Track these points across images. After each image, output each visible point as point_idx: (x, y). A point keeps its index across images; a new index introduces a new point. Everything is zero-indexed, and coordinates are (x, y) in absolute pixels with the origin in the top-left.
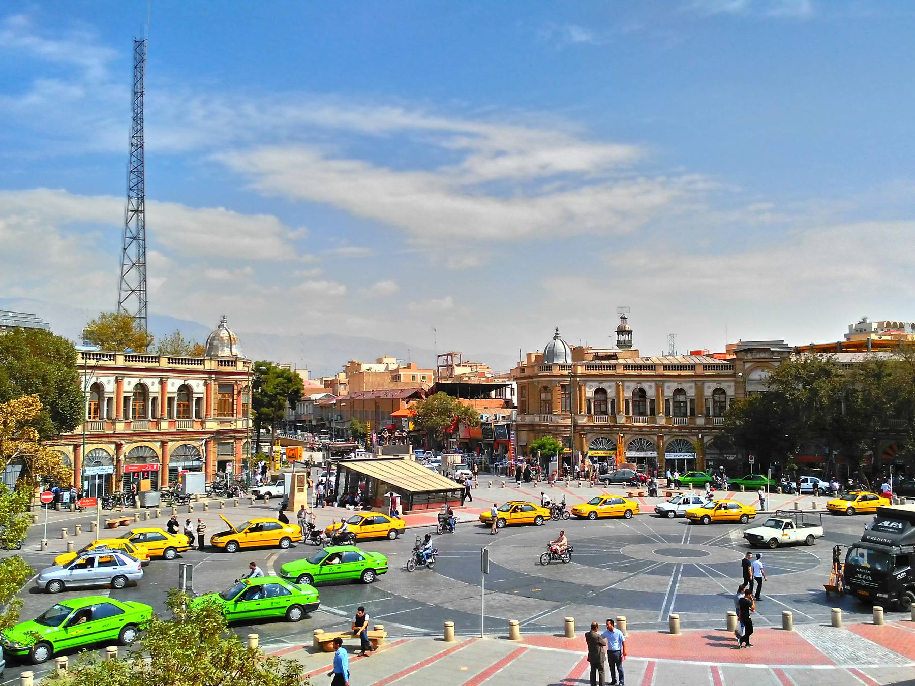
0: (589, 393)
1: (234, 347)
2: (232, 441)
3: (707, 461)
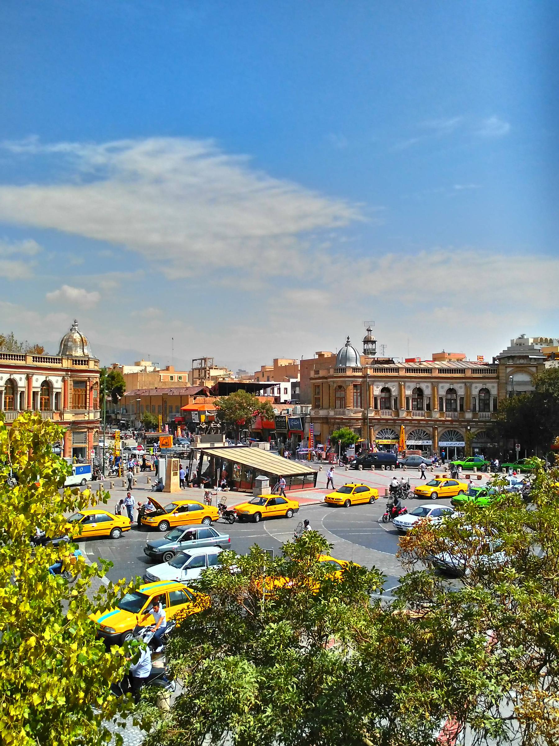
0: (376, 391)
1: (85, 347)
2: (86, 430)
3: (474, 448)
